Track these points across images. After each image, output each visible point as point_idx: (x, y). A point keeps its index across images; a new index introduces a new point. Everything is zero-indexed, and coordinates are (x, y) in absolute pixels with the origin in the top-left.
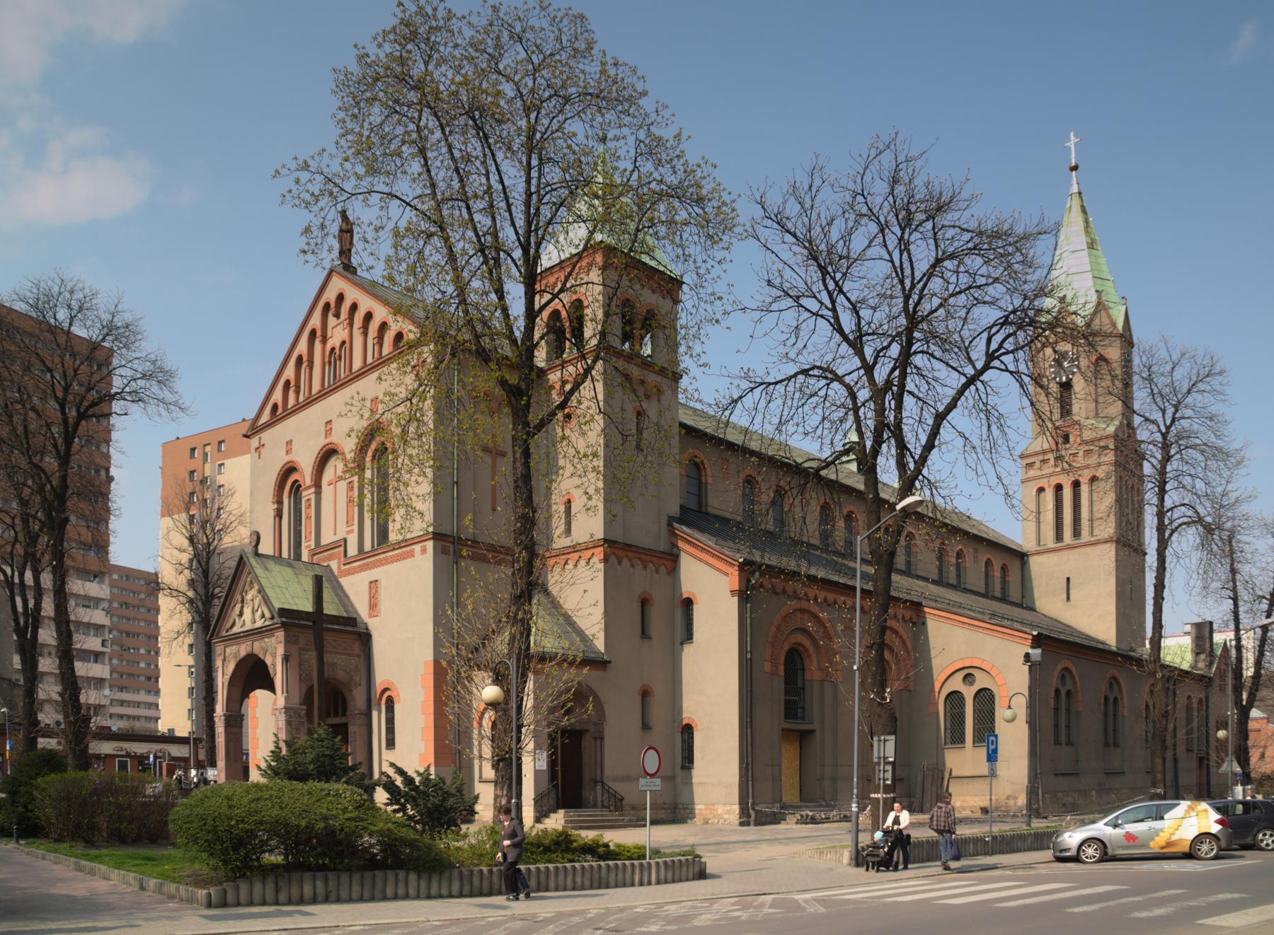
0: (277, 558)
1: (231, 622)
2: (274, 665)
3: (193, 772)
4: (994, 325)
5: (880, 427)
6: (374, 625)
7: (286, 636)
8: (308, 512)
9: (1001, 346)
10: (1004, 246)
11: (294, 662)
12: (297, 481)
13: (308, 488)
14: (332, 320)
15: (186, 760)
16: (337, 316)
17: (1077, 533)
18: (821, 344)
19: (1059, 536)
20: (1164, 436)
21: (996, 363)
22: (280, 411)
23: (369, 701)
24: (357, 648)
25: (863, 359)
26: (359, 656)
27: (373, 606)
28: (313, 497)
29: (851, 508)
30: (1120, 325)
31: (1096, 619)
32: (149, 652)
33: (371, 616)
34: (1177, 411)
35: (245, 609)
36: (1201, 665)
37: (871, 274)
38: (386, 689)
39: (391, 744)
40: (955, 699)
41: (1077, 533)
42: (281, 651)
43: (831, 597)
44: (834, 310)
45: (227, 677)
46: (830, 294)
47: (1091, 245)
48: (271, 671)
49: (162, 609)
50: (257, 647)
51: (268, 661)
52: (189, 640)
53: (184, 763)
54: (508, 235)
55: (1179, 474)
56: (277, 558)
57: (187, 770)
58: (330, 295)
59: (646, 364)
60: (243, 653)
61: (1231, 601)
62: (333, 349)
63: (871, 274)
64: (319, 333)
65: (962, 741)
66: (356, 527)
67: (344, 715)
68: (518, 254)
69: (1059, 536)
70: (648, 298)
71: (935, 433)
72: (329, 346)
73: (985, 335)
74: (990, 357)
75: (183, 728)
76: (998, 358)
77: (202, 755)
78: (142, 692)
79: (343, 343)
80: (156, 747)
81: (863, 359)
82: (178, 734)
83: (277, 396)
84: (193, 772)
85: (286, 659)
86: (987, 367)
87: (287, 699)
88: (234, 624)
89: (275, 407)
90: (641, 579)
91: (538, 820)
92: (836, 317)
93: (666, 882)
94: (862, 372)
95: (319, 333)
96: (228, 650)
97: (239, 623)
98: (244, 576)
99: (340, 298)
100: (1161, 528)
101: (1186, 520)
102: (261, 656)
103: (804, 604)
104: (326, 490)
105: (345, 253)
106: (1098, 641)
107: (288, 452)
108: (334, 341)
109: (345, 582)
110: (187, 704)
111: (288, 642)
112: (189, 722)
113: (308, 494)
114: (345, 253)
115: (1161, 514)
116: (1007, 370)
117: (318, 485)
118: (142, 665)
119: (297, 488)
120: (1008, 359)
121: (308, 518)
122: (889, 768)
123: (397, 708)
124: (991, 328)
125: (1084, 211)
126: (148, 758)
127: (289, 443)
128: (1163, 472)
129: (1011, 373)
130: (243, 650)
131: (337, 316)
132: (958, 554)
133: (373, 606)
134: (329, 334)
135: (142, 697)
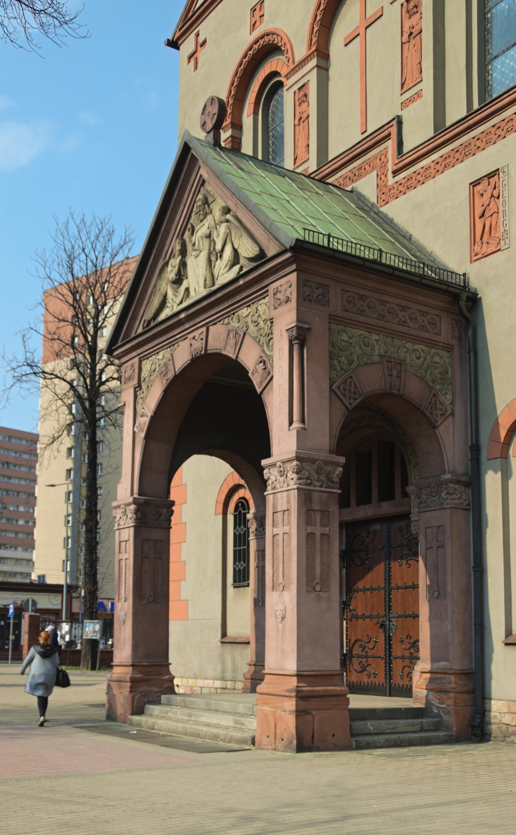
0: (254, 158)
2: (264, 362)
3: (65, 627)
7: (301, 284)
11: (318, 344)
12: (275, 74)
15: (57, 613)
23: (475, 450)
24: (446, 330)
26: (449, 348)
32: (27, 522)
33: (476, 257)
35: (190, 261)
42: (287, 318)
45: (144, 421)
49: (39, 480)
50: (218, 337)
51: (249, 358)
52: (67, 442)
53: (55, 616)
56: (254, 158)
57: (57, 624)
66: (427, 85)
75: (57, 577)
77: (77, 607)
78: (20, 549)
80: (21, 597)
82: (49, 581)
84: (65, 627)
85: (300, 338)
87: (301, 434)
96: (147, 366)
98: (187, 197)
110: (62, 554)
111: (305, 299)
112: (64, 551)
117: (322, 52)
118: (21, 522)
126: (8, 610)
130: (182, 354)
135: (20, 553)
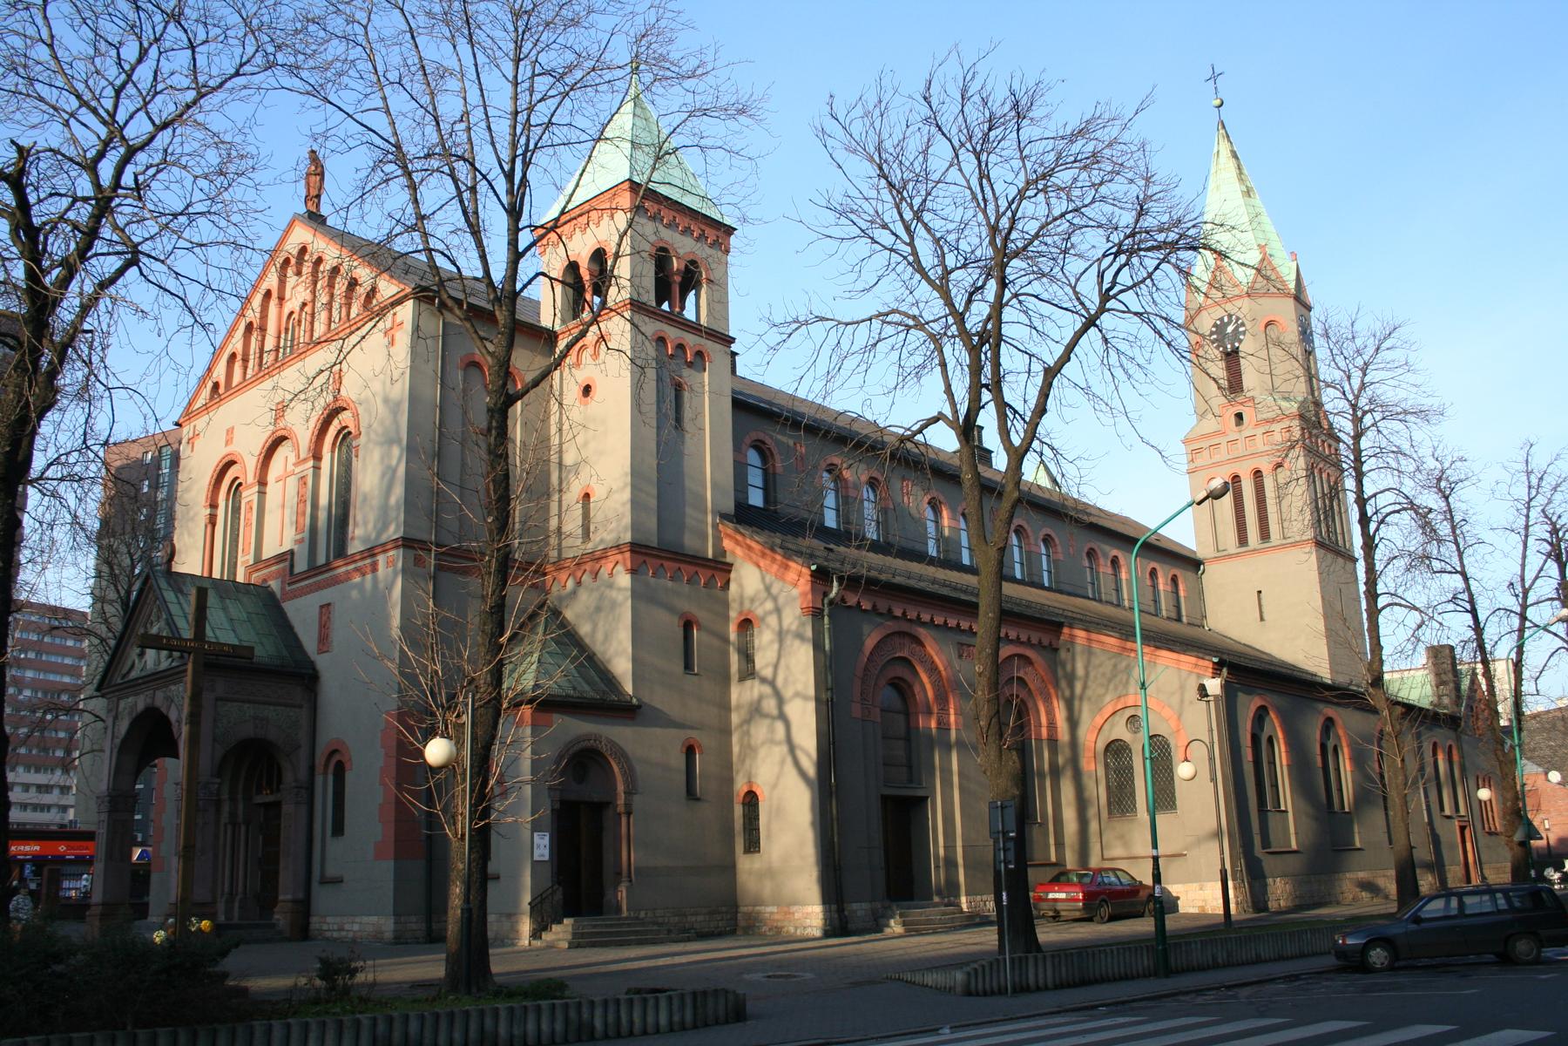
1: (129, 663)
2: (179, 722)
4: (1104, 256)
5: (975, 388)
6: (322, 662)
8: (248, 517)
9: (1114, 283)
10: (1091, 151)
13: (251, 486)
14: (292, 280)
16: (299, 273)
17: (1265, 534)
18: (898, 290)
19: (1243, 540)
20: (1354, 407)
21: (1111, 304)
22: (221, 391)
25: (949, 303)
27: (324, 640)
28: (255, 497)
29: (1049, 531)
30: (1292, 285)
31: (1298, 640)
33: (320, 652)
34: (1365, 375)
36: (1446, 701)
37: (951, 208)
38: (335, 751)
39: (338, 829)
40: (1117, 750)
41: (1265, 534)
43: (883, 605)
44: (911, 244)
46: (907, 228)
47: (1248, 193)
48: (175, 730)
50: (159, 700)
54: (486, 159)
55: (1380, 452)
58: (292, 247)
59: (694, 328)
60: (141, 707)
61: (1469, 616)
62: (292, 313)
63: (951, 208)
64: (275, 294)
65: (1133, 808)
67: (278, 790)
68: (501, 185)
69: (1243, 540)
70: (684, 246)
71: (1044, 394)
72: (286, 312)
73: (1094, 270)
74: (1105, 297)
76: (1114, 297)
79: (304, 304)
81: (949, 303)
83: (220, 372)
86: (1102, 309)
88: (133, 666)
89: (216, 386)
90: (684, 595)
91: (536, 934)
92: (915, 253)
93: (683, 1028)
94: (951, 320)
95: (275, 294)
97: (138, 666)
99: (303, 250)
100: (1364, 520)
101: (1398, 507)
102: (164, 710)
103: (905, 627)
104: (273, 489)
105: (314, 197)
106: (1307, 672)
107: (227, 444)
108: (292, 304)
109: (289, 607)
113: (249, 495)
114: (314, 197)
115: (1362, 502)
116: (1129, 311)
117: (262, 483)
119: (237, 487)
120: (1128, 297)
121: (248, 524)
122: (1011, 845)
123: (349, 777)
124: (1099, 260)
125: (1235, 155)
127: (230, 431)
128: (1357, 452)
129: (1136, 314)
130: (141, 703)
131: (299, 273)
132: (1089, 554)
133: (324, 640)
134: (287, 296)
